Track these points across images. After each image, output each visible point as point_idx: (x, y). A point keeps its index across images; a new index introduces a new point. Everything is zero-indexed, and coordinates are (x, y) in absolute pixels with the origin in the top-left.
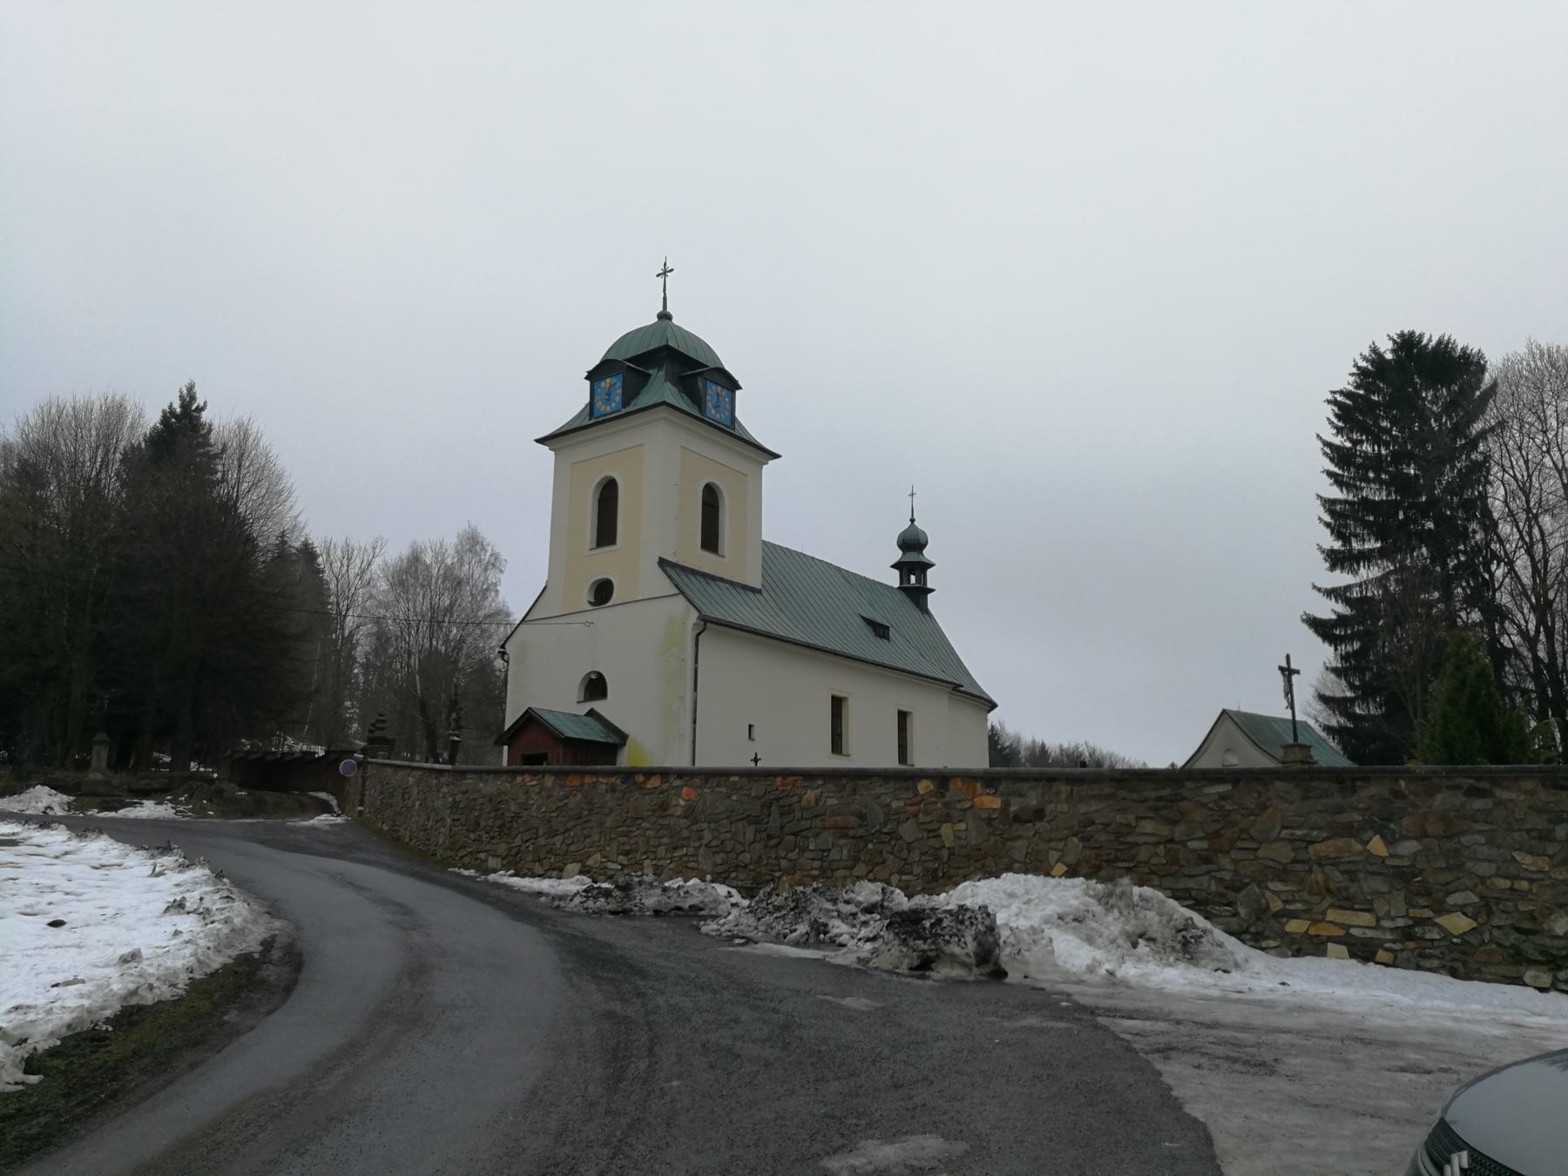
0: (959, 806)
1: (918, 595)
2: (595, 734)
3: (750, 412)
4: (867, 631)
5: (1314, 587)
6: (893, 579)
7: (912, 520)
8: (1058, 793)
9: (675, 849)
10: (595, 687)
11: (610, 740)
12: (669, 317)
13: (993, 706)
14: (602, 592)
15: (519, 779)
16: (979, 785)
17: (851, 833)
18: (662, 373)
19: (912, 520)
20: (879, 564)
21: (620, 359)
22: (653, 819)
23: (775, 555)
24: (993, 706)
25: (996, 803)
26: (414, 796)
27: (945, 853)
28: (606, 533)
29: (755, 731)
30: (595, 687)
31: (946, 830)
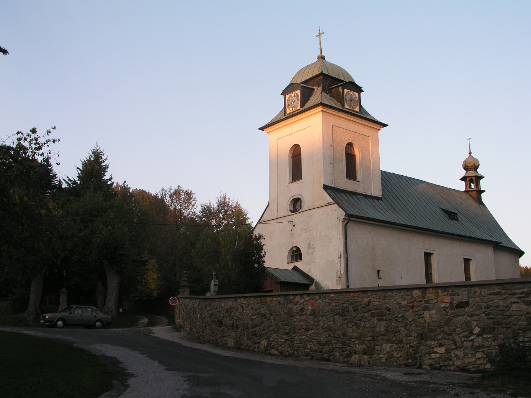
0: (431, 302)
1: (476, 194)
2: (297, 279)
3: (369, 102)
4: (445, 217)
5: (262, 129)
6: (461, 187)
7: (470, 153)
8: (475, 292)
9: (308, 330)
10: (296, 254)
11: (307, 283)
12: (323, 58)
13: (521, 253)
14: (296, 204)
15: (239, 300)
16: (440, 291)
17: (384, 318)
18: (320, 88)
19: (470, 153)
20: (453, 180)
21: (298, 82)
22: (298, 317)
23: (387, 178)
24: (521, 253)
25: (448, 299)
26: (198, 312)
27: (426, 325)
28: (296, 174)
29: (381, 273)
30: (296, 254)
31: (426, 314)
